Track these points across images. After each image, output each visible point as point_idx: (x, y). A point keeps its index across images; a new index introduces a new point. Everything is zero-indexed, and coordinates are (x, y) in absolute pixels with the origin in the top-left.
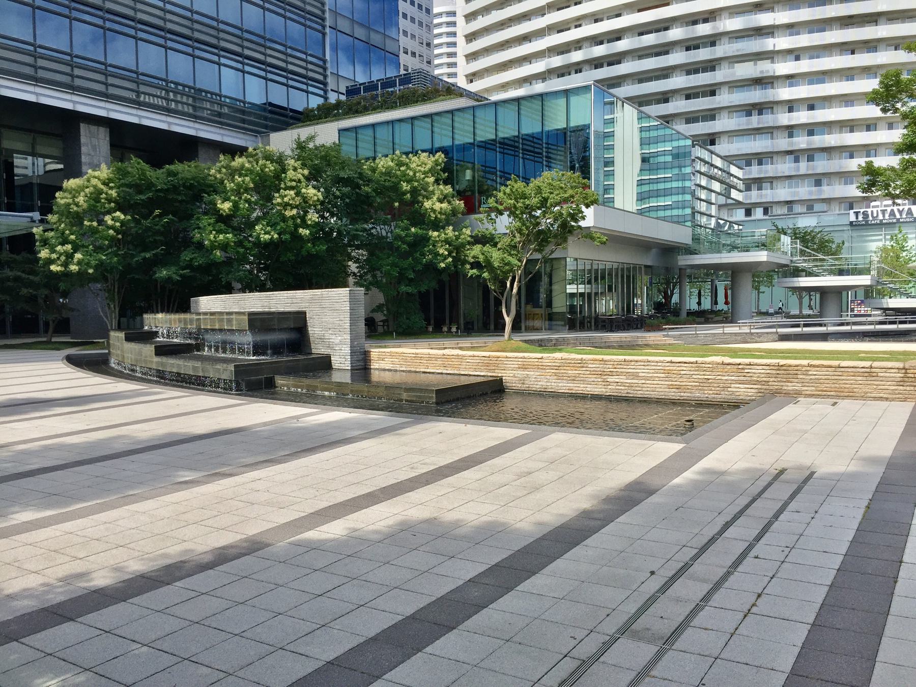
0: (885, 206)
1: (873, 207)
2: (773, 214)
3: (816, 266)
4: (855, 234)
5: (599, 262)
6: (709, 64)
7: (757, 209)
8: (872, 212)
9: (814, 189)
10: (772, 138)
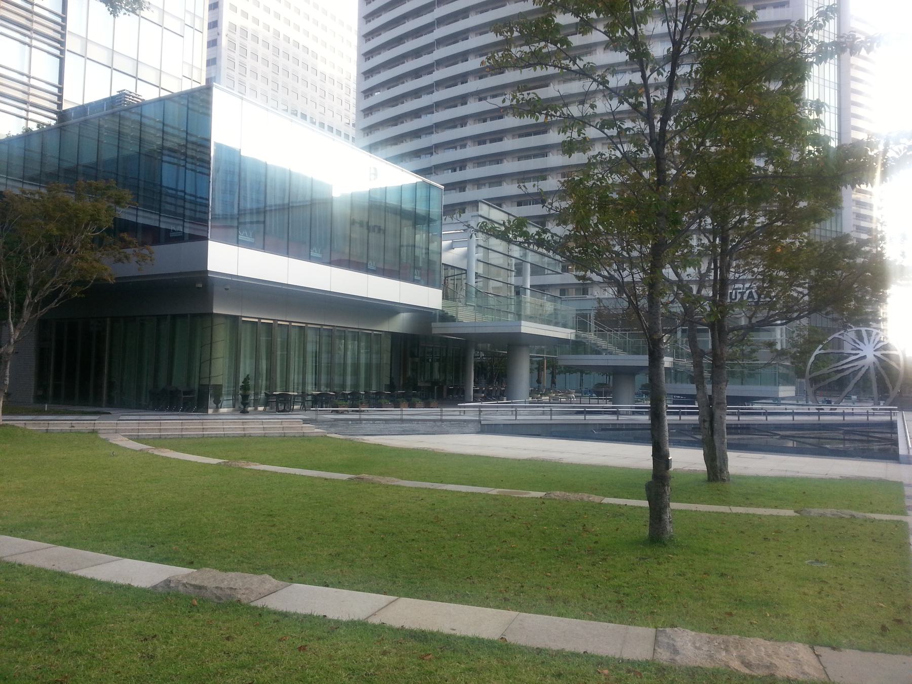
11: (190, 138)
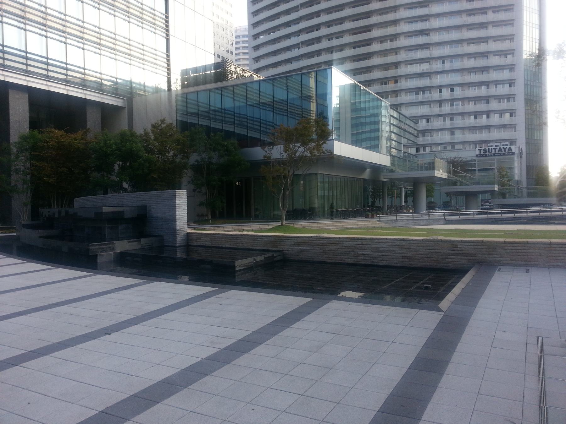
0: (496, 146)
1: (489, 146)
2: (433, 150)
8: (489, 149)
10: (430, 79)
11: (275, 99)
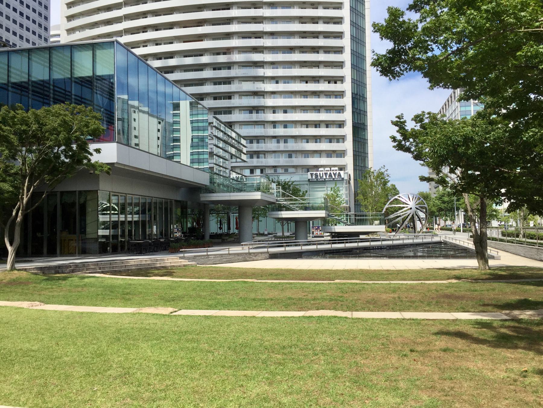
0: (326, 171)
3: (292, 204)
4: (312, 186)
5: (134, 196)
6: (227, 80)
7: (257, 170)
9: (288, 159)
10: (264, 128)
